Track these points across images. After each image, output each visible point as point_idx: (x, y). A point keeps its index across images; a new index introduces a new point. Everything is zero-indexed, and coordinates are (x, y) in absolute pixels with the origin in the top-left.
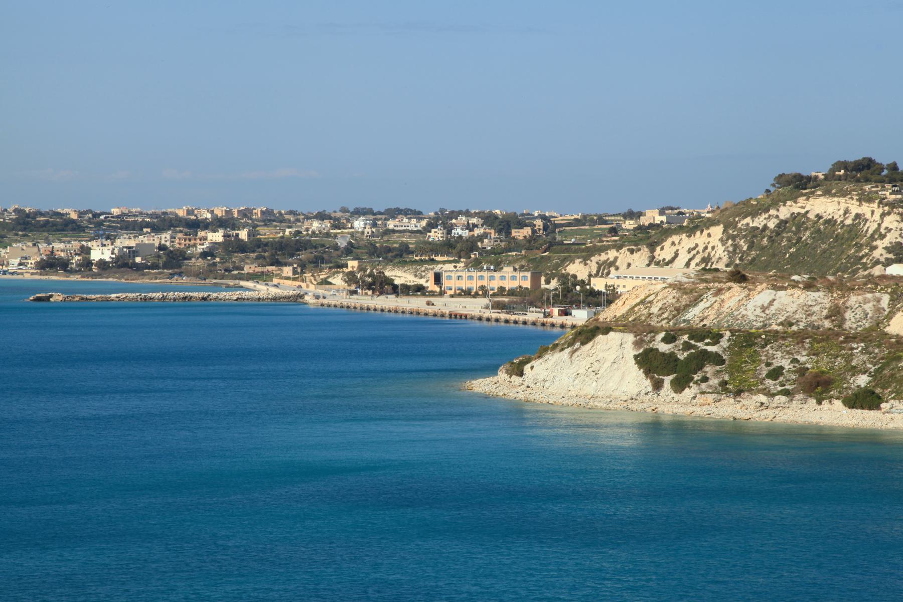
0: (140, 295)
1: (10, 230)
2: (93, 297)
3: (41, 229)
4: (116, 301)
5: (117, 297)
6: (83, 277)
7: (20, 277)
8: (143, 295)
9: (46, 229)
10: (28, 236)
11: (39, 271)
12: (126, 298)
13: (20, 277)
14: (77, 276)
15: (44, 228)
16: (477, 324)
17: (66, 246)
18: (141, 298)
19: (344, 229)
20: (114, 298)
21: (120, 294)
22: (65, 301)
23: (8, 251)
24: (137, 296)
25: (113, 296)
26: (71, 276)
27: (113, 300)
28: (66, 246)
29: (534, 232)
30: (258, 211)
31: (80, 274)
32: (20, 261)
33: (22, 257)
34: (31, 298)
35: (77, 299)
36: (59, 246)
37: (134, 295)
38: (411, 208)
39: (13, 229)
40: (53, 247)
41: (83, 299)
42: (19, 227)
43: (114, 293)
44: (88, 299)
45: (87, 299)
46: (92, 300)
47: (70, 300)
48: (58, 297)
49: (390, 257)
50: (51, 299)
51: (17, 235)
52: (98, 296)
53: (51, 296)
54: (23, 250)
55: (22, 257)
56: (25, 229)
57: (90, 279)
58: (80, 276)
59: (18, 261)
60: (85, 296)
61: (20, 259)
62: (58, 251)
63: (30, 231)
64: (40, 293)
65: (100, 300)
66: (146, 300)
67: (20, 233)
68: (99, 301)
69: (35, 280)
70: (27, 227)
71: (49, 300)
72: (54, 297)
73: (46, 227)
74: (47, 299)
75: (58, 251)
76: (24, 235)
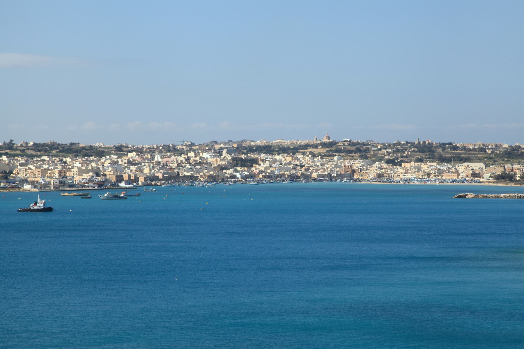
0: (518, 195)
1: (501, 158)
2: (491, 195)
3: (519, 157)
4: (503, 198)
5: (504, 196)
6: (515, 184)
7: (482, 184)
8: (519, 194)
9: (521, 157)
10: (510, 161)
11: (495, 181)
12: (509, 196)
13: (482, 184)
14: (512, 184)
15: (520, 156)
16: (28, 192)
17: (520, 167)
18: (518, 197)
19: (475, 151)
20: (502, 197)
21: (506, 194)
22: (474, 198)
23: (487, 170)
24: (516, 195)
25: (502, 195)
26: (509, 184)
27: (501, 198)
28: (520, 167)
29: (48, 150)
30: (32, 143)
31: (514, 183)
32: (490, 175)
33: (491, 173)
34: (456, 196)
35: (481, 197)
36: (516, 167)
37: (514, 194)
38: (60, 141)
39: (502, 157)
40: (513, 167)
41: (484, 197)
42: (506, 156)
43: (503, 194)
44: (488, 197)
45: (487, 197)
46: (490, 197)
47: (477, 197)
48: (470, 196)
49: (183, 166)
50: (466, 197)
51: (503, 160)
52: (493, 195)
53: (467, 195)
54: (495, 169)
55: (491, 173)
56: (509, 157)
57: (519, 186)
58: (514, 184)
59: (489, 175)
60: (486, 195)
61: (490, 174)
62: (516, 169)
63: (512, 158)
64: (461, 193)
65: (494, 197)
66: (521, 197)
67: (506, 159)
68: (493, 198)
69: (490, 186)
70: (511, 156)
71: (465, 197)
72: (468, 195)
73: (521, 156)
74: (464, 197)
75: (516, 169)
76: (507, 161)
